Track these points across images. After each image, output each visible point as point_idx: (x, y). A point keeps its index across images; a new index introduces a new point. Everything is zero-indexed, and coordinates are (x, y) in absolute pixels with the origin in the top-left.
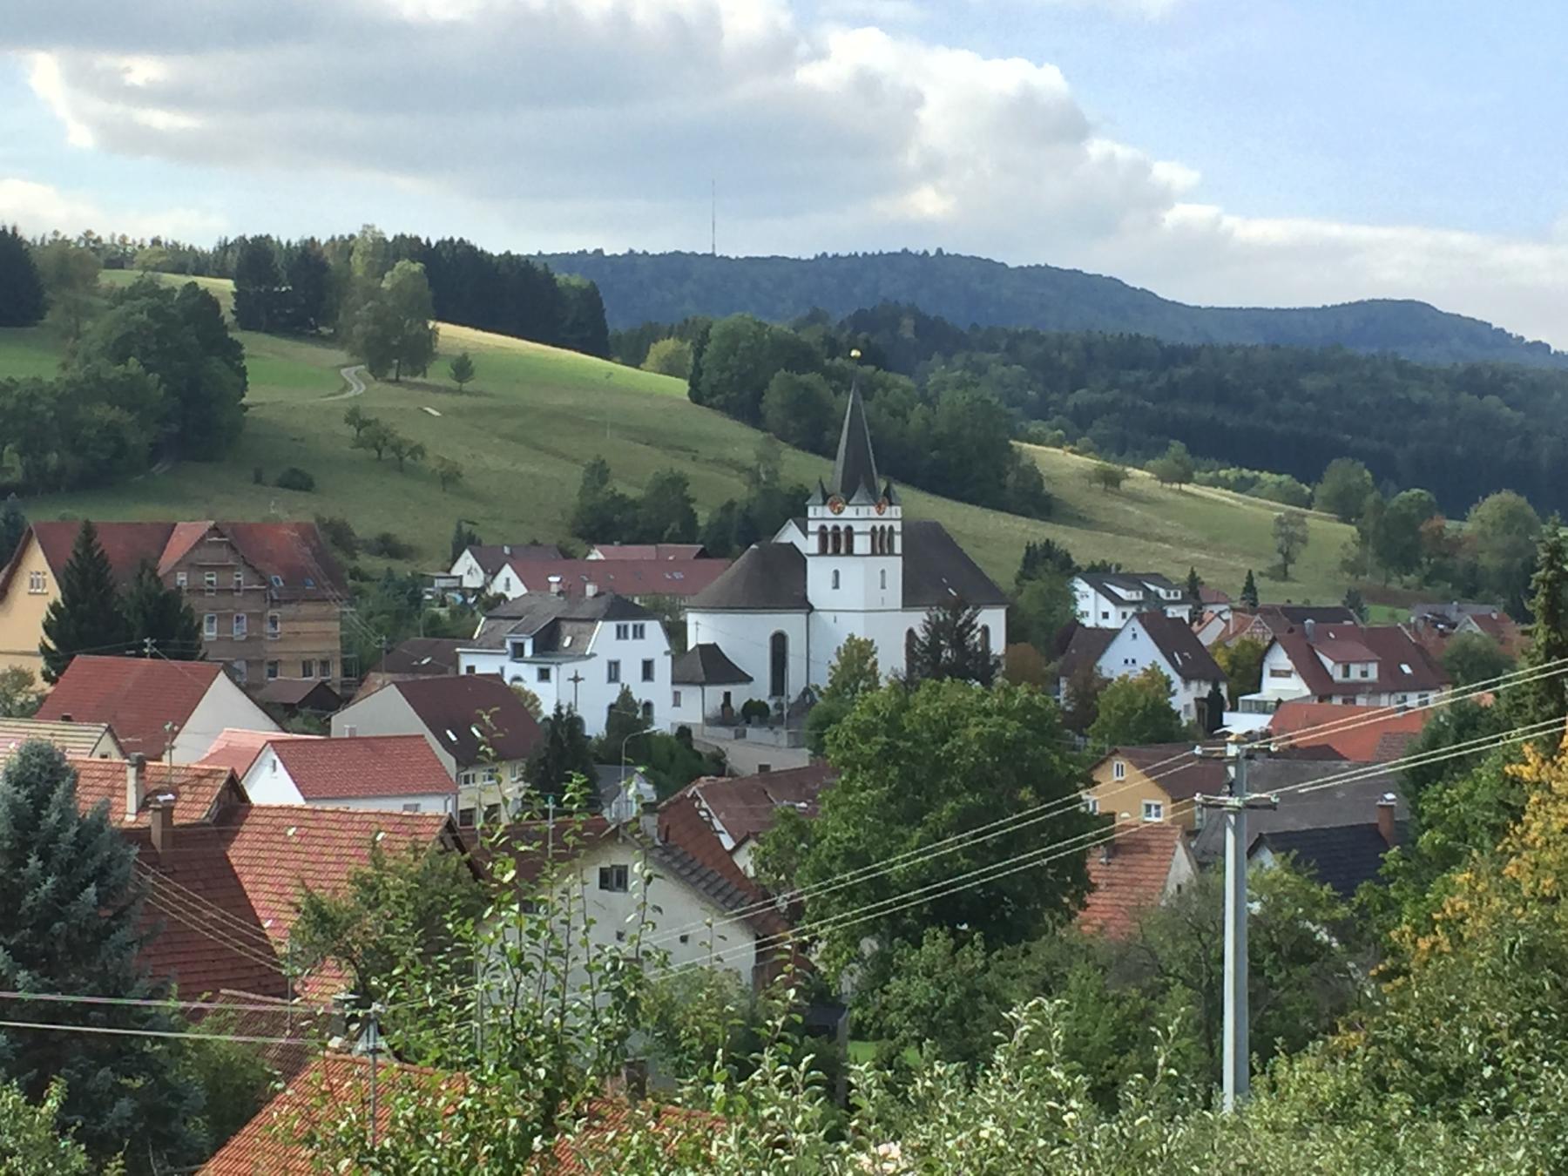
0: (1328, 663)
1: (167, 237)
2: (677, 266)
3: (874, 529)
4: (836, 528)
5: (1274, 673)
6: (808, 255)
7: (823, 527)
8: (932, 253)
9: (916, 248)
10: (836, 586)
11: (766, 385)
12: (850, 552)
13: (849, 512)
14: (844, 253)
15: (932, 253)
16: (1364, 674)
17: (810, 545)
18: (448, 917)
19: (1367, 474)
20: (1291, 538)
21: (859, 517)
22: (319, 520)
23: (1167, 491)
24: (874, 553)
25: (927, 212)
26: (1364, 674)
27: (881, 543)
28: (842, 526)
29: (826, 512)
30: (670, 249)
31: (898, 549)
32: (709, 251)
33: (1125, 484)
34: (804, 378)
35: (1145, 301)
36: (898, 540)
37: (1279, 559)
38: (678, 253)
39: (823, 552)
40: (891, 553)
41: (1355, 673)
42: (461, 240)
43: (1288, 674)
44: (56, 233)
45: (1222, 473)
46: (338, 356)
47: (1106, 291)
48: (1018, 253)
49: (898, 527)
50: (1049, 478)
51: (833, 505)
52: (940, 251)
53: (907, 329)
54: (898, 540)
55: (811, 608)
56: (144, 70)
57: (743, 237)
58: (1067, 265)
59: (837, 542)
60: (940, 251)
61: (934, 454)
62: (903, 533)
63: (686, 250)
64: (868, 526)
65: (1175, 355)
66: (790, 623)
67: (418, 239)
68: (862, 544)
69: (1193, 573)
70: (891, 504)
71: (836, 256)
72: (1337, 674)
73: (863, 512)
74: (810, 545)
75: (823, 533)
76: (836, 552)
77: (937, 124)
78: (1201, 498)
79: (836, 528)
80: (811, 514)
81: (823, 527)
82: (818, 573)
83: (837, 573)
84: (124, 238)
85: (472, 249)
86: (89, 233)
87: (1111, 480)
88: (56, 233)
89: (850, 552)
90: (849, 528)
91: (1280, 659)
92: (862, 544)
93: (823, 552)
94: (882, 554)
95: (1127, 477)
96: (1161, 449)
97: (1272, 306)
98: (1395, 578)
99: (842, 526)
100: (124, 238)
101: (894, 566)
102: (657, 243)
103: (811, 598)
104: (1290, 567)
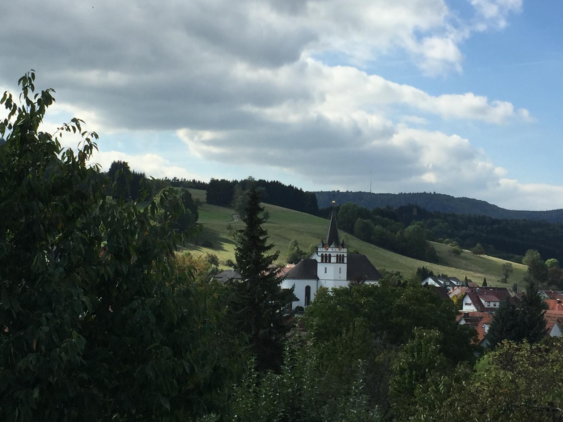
0: (483, 301)
1: (197, 180)
2: (360, 195)
3: (337, 255)
4: (326, 254)
5: (466, 304)
6: (397, 193)
7: (322, 254)
8: (432, 193)
9: (428, 191)
10: (326, 272)
11: (355, 223)
12: (330, 262)
13: (330, 250)
14: (407, 193)
15: (432, 193)
16: (495, 305)
17: (319, 259)
18: (395, 407)
19: (538, 254)
20: (507, 271)
21: (333, 251)
22: (208, 255)
23: (475, 257)
24: (337, 262)
25: (429, 180)
26: (495, 305)
27: (340, 260)
28: (328, 254)
29: (324, 250)
30: (367, 191)
31: (345, 261)
32: (369, 191)
33: (462, 254)
34: (365, 221)
35: (494, 208)
36: (345, 259)
37: (504, 277)
38: (360, 192)
39: (322, 262)
40: (343, 263)
41: (492, 305)
42: (277, 181)
43: (470, 304)
44: (166, 178)
45: (503, 255)
46: (232, 211)
47: (483, 204)
48: (457, 194)
49: (345, 255)
50: (439, 252)
51: (325, 247)
52: (434, 193)
53: (415, 212)
54: (345, 259)
55: (318, 279)
56: (208, 135)
57: (379, 188)
58: (471, 197)
59: (326, 259)
60: (434, 193)
61: (404, 244)
62: (347, 257)
63: (363, 191)
64: (335, 254)
65: (494, 222)
66: (312, 283)
67: (265, 181)
68: (333, 260)
69: (466, 277)
70: (343, 248)
71: (405, 194)
72: (486, 304)
73: (334, 250)
74: (319, 259)
75: (322, 256)
76: (326, 262)
77: (429, 157)
78: (482, 258)
79: (326, 254)
80: (319, 250)
81: (322, 254)
82: (321, 268)
83: (326, 268)
84: (185, 180)
85: (280, 184)
86: (175, 178)
87: (457, 253)
88: (166, 178)
89: (330, 262)
90: (330, 255)
91: (468, 300)
92: (333, 260)
93: (322, 262)
94: (340, 263)
95: (462, 252)
96: (474, 245)
97: (531, 210)
98: (540, 283)
99: (328, 254)
100: (185, 180)
101: (344, 267)
102: (354, 189)
103: (318, 276)
104: (507, 279)
